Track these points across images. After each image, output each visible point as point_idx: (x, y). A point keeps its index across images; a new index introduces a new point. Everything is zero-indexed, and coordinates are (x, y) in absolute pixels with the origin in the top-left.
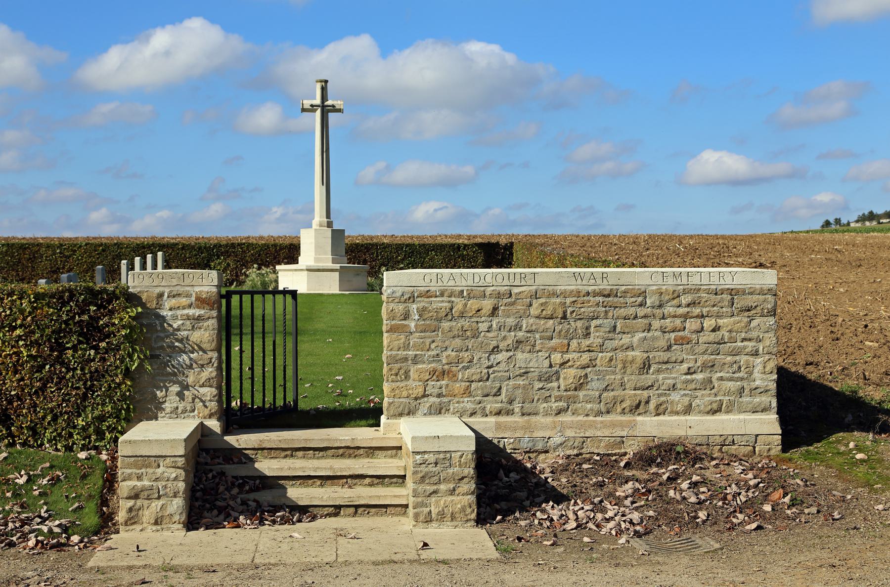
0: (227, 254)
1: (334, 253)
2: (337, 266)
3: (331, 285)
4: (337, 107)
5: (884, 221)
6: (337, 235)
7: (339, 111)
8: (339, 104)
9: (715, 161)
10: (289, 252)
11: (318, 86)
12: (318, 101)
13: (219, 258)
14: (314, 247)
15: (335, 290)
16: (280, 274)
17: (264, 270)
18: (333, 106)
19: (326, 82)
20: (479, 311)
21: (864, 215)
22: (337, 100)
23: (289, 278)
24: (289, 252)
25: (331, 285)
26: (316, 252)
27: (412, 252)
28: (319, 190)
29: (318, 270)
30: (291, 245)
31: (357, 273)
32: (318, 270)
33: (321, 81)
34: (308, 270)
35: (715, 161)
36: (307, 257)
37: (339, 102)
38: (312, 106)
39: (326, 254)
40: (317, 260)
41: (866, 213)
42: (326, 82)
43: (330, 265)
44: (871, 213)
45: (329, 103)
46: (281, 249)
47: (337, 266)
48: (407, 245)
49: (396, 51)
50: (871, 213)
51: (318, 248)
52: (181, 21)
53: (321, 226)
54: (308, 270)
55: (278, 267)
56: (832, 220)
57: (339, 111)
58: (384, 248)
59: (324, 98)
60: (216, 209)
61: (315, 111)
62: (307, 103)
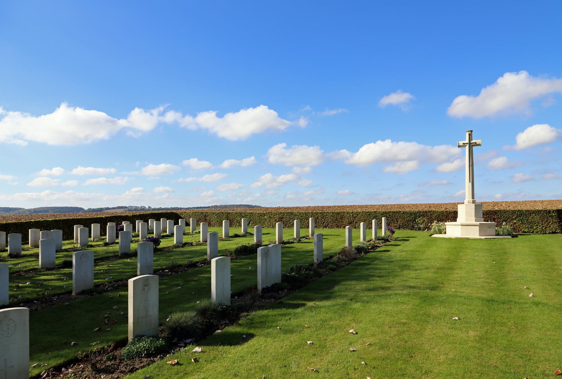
0: (423, 216)
1: (476, 215)
2: (478, 223)
3: (474, 233)
6: (478, 207)
8: (478, 141)
10: (452, 216)
11: (467, 134)
12: (467, 141)
13: (419, 217)
14: (466, 213)
15: (477, 236)
16: (447, 227)
17: (441, 223)
19: (471, 131)
20: (433, 288)
23: (453, 230)
24: (452, 216)
25: (474, 233)
26: (211, 277)
28: (468, 185)
29: (467, 225)
31: (490, 226)
32: (467, 225)
36: (461, 218)
40: (466, 220)
43: (474, 222)
45: (473, 141)
46: (450, 213)
47: (478, 223)
48: (518, 211)
49: (319, 147)
51: (467, 214)
52: (277, 144)
53: (469, 203)
55: (446, 223)
57: (479, 145)
60: (407, 199)
61: (465, 146)
62: (461, 143)
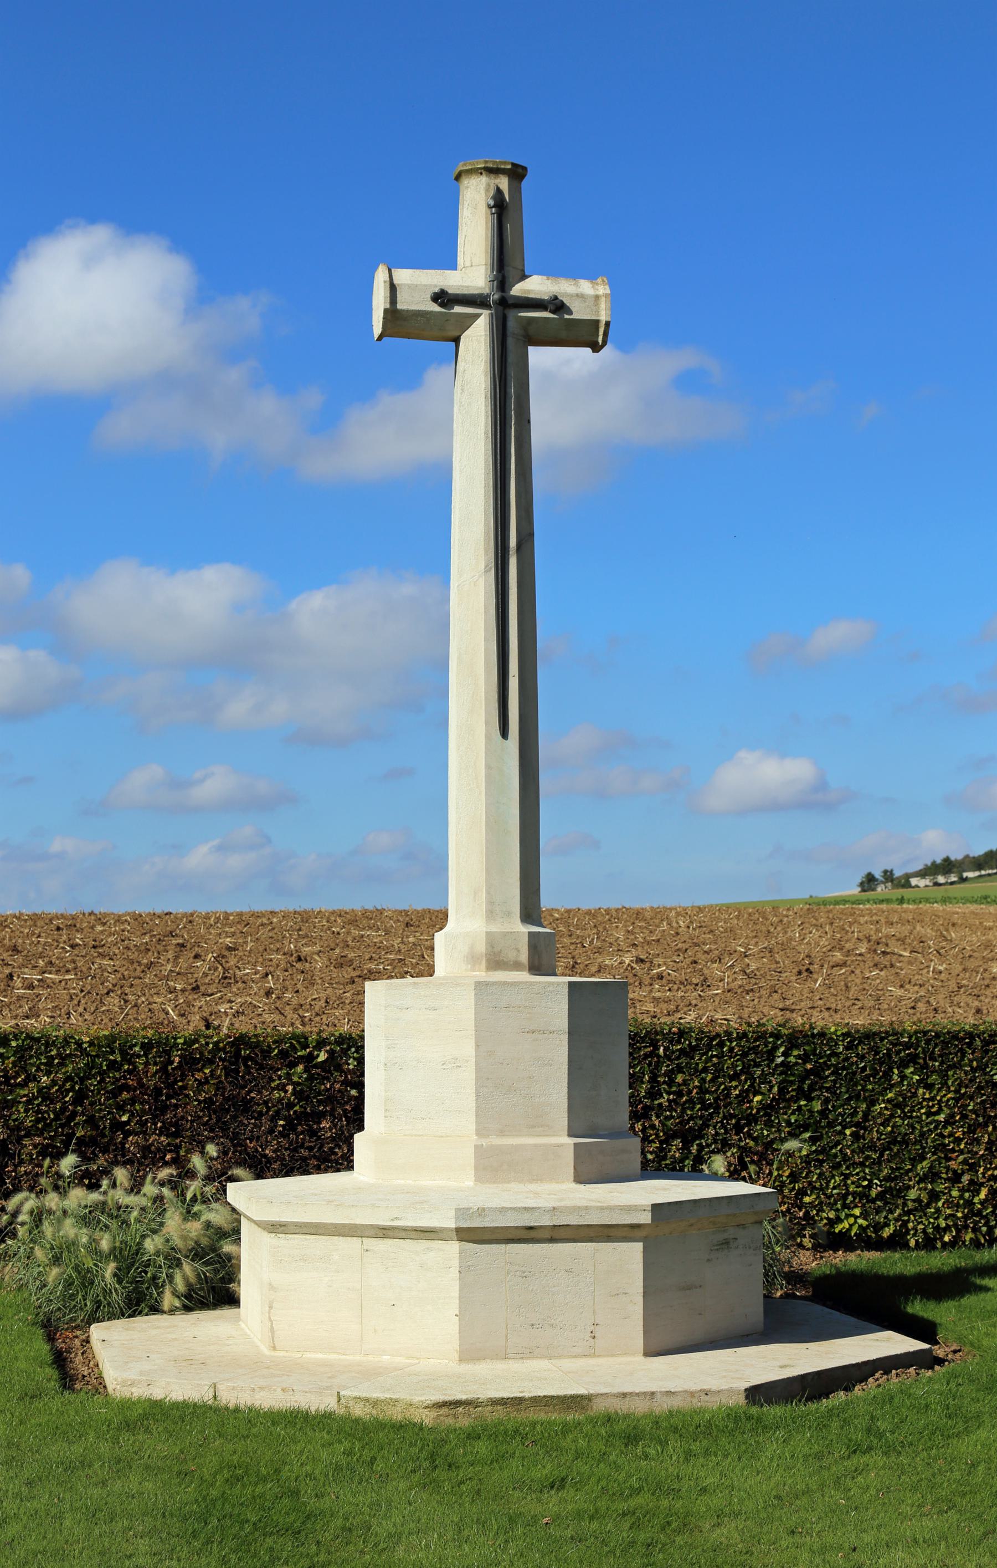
4: (579, 312)
5: (970, 875)
7: (587, 336)
8: (587, 296)
9: (771, 772)
10: (301, 1106)
12: (472, 271)
18: (557, 305)
19: (517, 173)
21: (934, 863)
22: (574, 275)
27: (817, 1072)
29: (528, 1235)
30: (241, 1040)
32: (528, 1235)
33: (492, 171)
34: (467, 1235)
35: (771, 772)
37: (585, 287)
38: (442, 297)
39: (538, 1124)
41: (929, 864)
42: (517, 173)
44: (947, 860)
47: (642, 1196)
48: (794, 1039)
50: (947, 860)
54: (467, 1235)
55: (246, 1194)
56: (878, 875)
58: (688, 1053)
59: (505, 263)
